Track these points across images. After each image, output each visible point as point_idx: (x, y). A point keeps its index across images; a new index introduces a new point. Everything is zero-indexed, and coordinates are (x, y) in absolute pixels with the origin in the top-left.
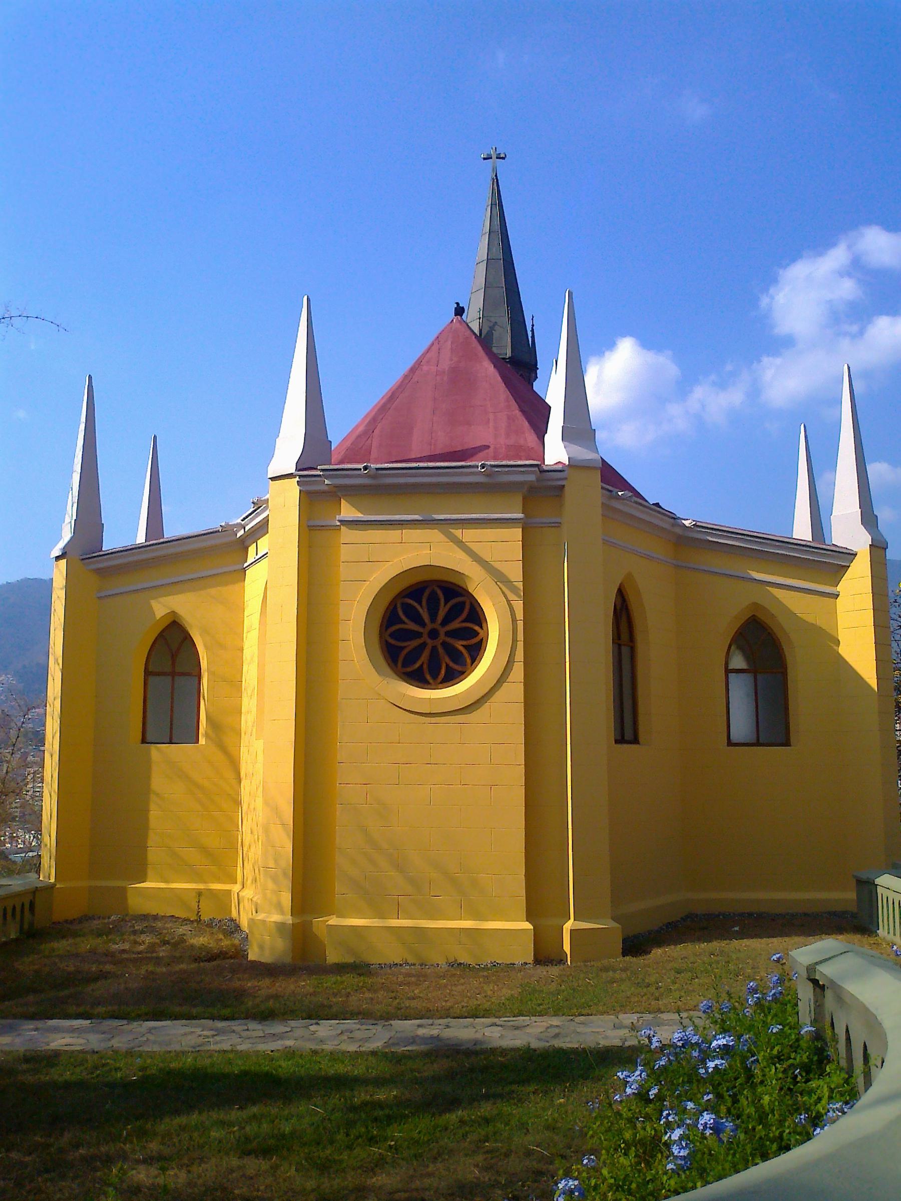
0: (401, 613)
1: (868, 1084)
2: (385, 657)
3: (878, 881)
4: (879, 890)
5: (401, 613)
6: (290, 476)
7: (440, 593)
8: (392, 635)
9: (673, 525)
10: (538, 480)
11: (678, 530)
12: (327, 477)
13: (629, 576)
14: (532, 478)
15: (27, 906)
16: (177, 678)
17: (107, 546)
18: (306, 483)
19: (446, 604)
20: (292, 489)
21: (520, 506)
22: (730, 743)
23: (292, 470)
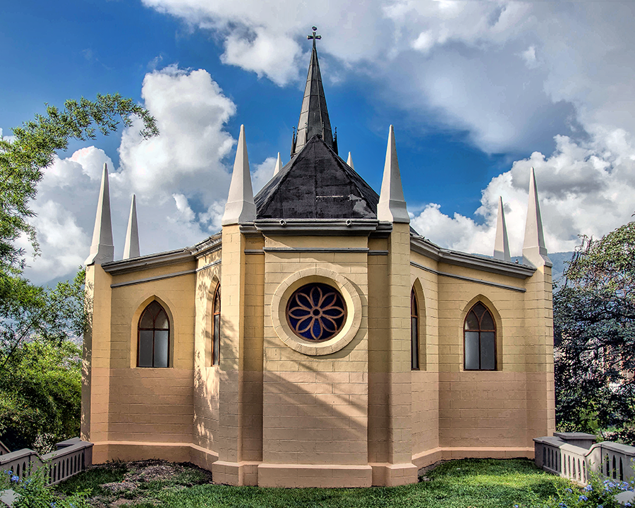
6: (236, 224)
14: (374, 228)
19: (334, 319)
22: (465, 369)
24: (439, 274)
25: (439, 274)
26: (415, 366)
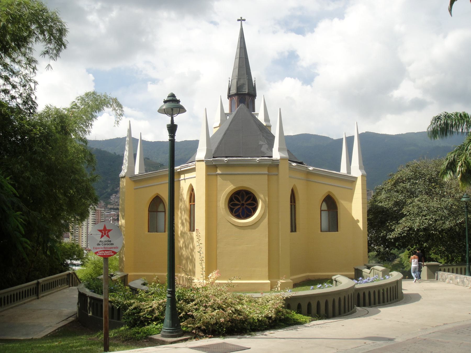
0: (234, 199)
1: (351, 310)
2: (230, 211)
3: (363, 270)
4: (363, 273)
5: (234, 199)
6: (203, 161)
7: (252, 198)
8: (231, 205)
9: (306, 169)
10: (272, 163)
11: (308, 170)
12: (214, 162)
13: (294, 185)
14: (270, 163)
15: (29, 290)
16: (158, 213)
17: (135, 174)
18: (207, 163)
20: (203, 165)
21: (267, 171)
23: (204, 159)
24: (307, 180)
25: (307, 180)
26: (294, 230)
